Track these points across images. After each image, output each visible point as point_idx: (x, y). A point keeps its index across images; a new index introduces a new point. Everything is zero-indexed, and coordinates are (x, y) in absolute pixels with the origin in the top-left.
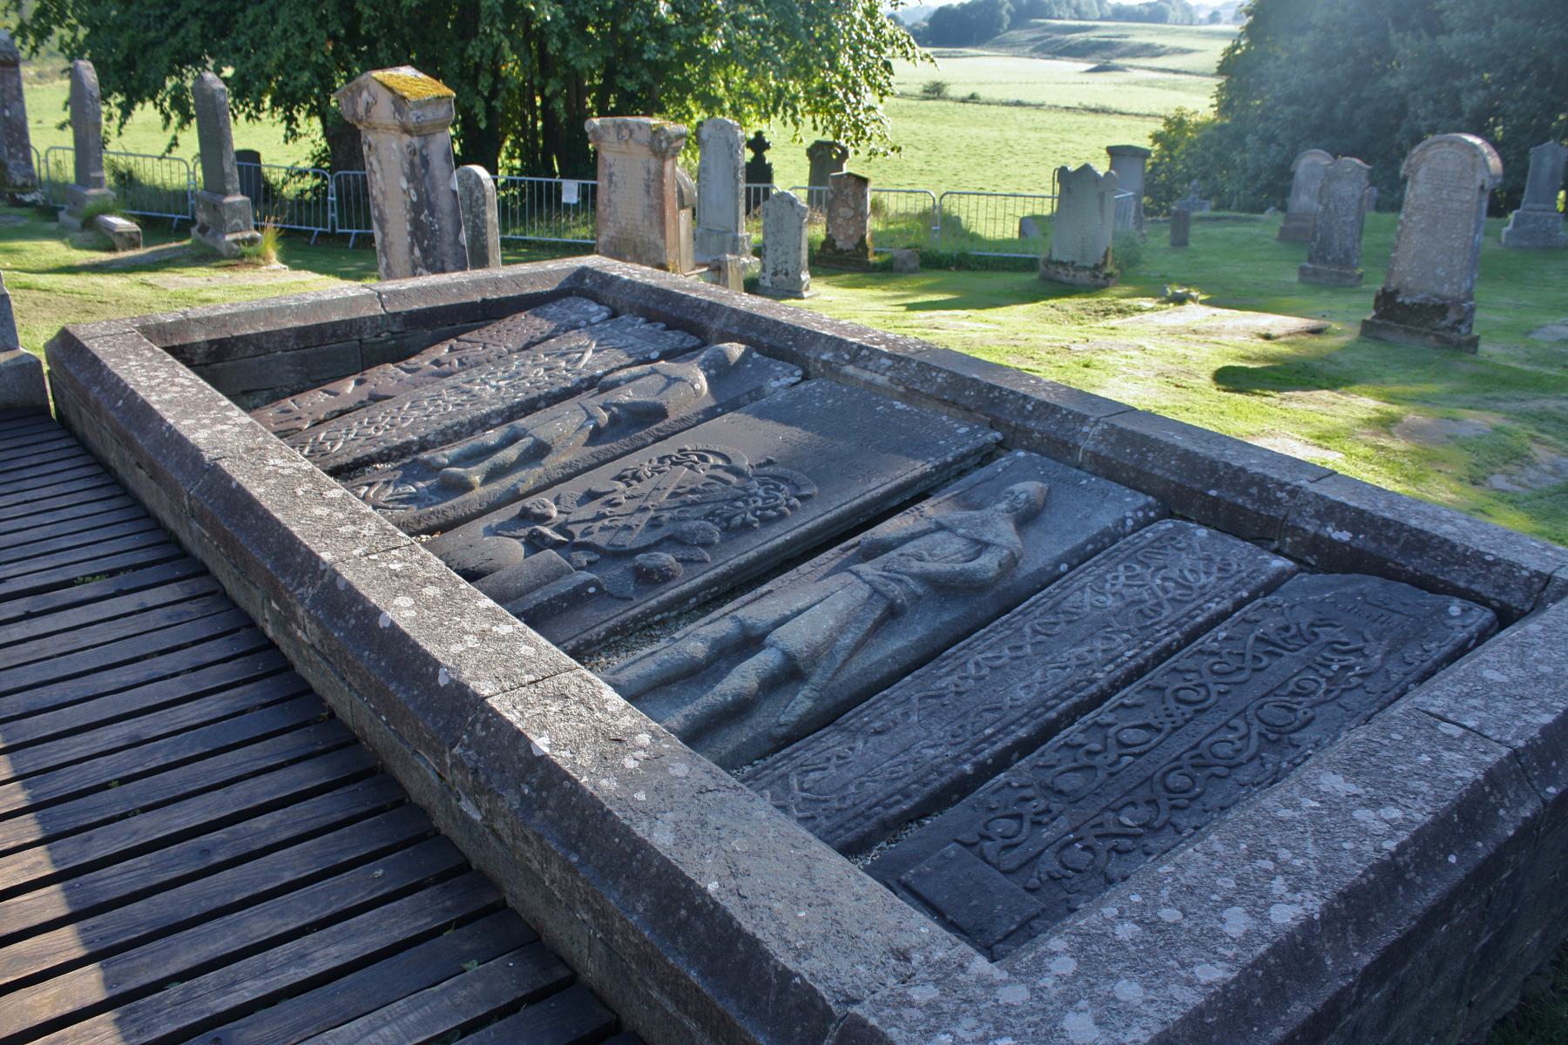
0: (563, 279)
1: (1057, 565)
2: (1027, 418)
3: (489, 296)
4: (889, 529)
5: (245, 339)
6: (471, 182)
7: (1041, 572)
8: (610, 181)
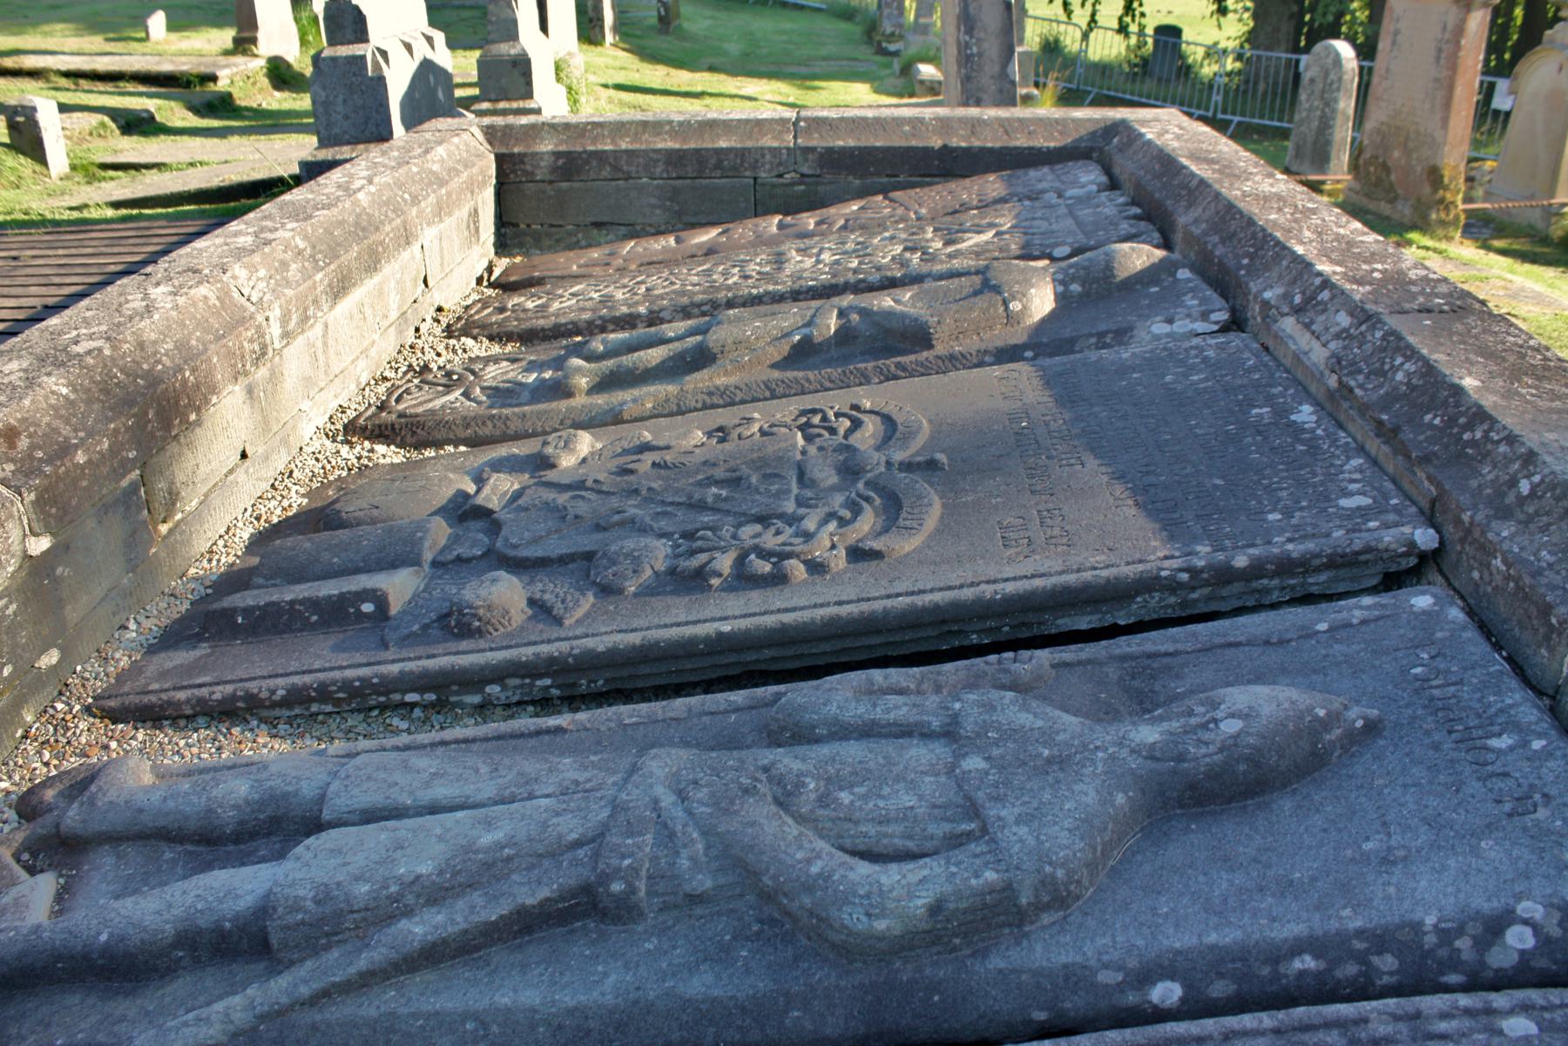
0: (1083, 132)
1: (1145, 977)
2: (1504, 513)
3: (954, 142)
4: (839, 695)
5: (600, 156)
6: (1330, 61)
7: (1074, 977)
8: (1394, 43)
